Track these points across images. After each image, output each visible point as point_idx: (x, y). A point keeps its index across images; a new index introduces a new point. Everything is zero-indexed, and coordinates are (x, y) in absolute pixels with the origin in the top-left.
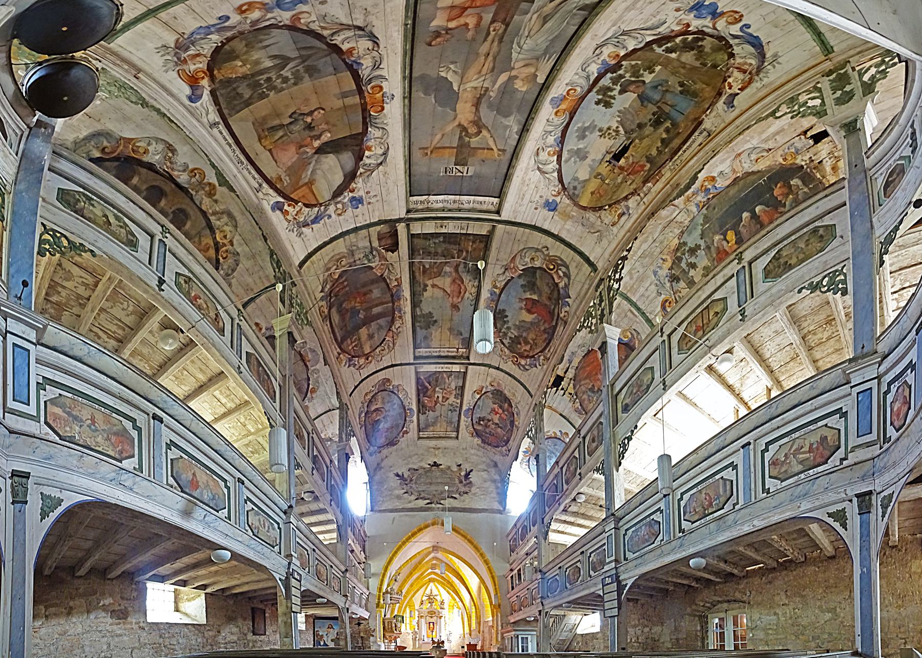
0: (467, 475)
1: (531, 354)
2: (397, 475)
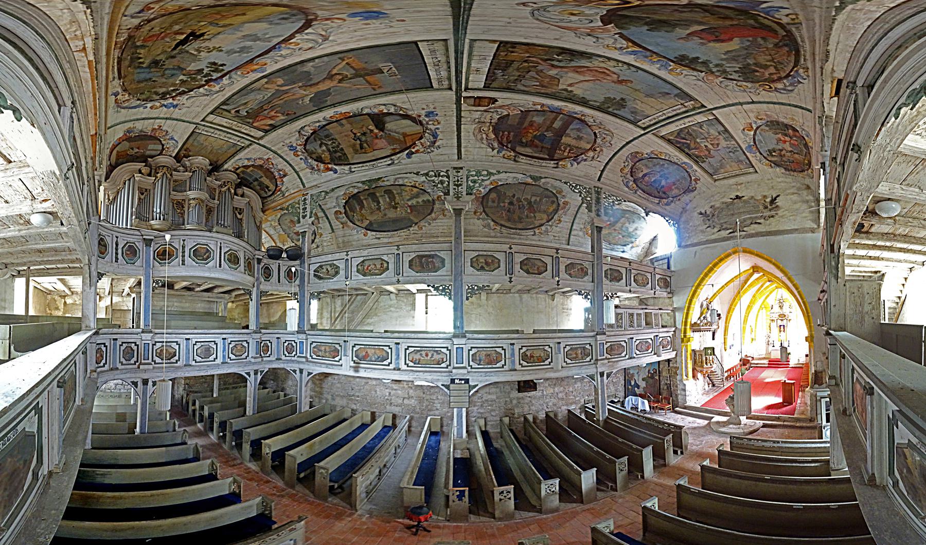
0: (773, 201)
1: (783, 75)
2: (701, 214)
